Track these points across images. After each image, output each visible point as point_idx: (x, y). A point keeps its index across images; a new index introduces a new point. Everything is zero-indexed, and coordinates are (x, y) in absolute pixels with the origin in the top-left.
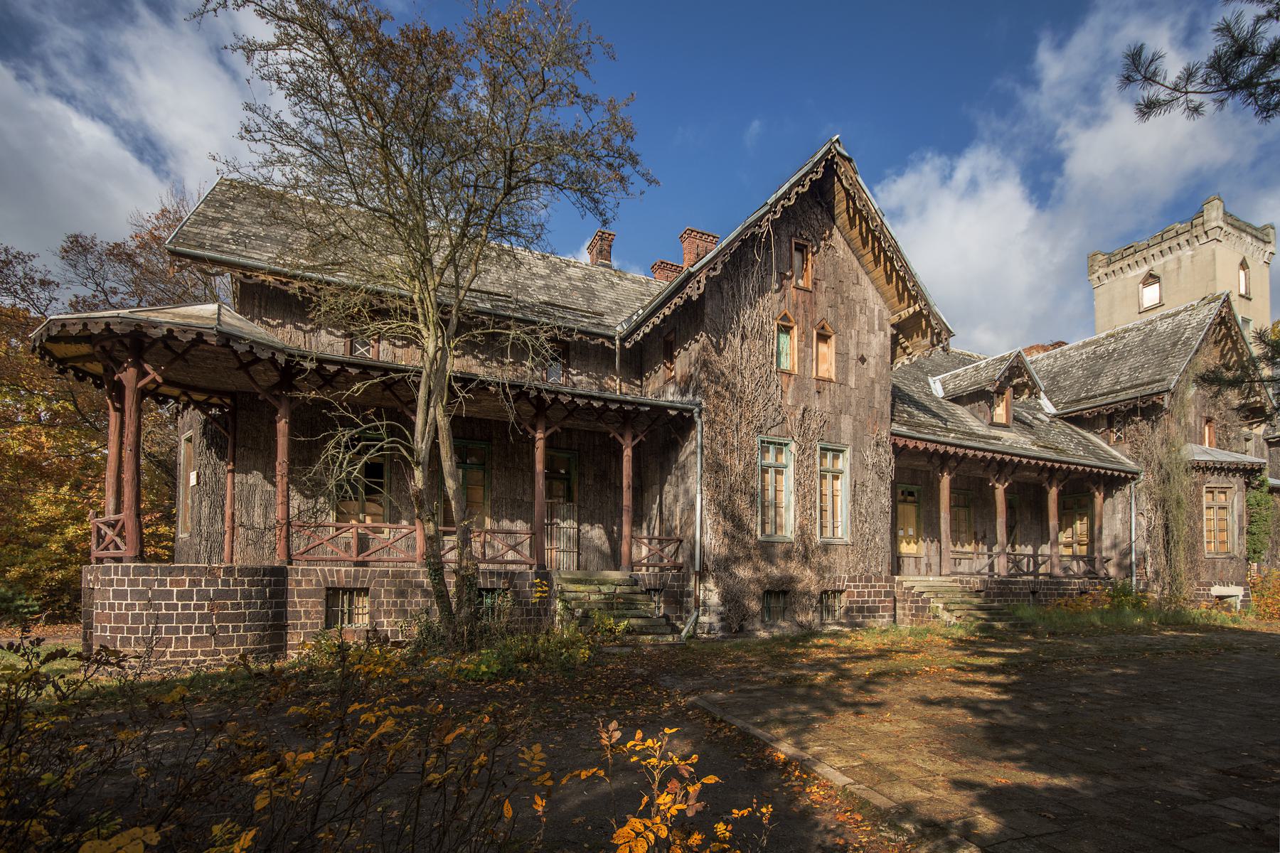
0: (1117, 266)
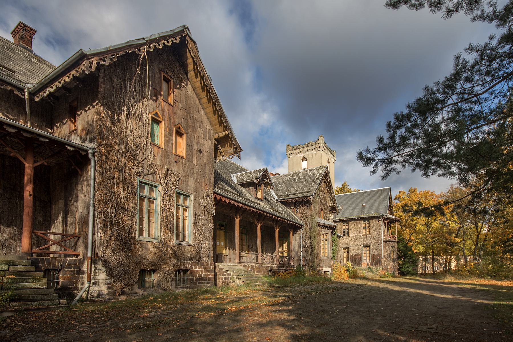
0: (295, 151)
